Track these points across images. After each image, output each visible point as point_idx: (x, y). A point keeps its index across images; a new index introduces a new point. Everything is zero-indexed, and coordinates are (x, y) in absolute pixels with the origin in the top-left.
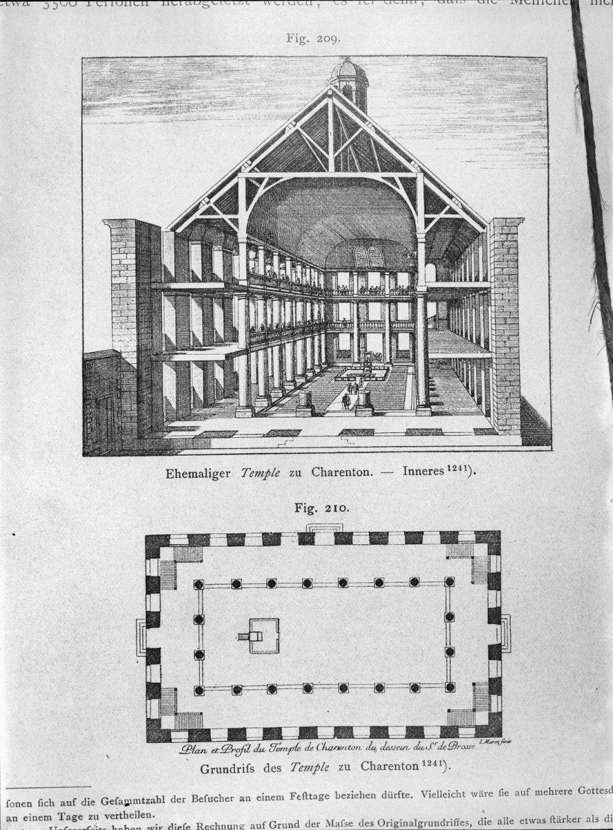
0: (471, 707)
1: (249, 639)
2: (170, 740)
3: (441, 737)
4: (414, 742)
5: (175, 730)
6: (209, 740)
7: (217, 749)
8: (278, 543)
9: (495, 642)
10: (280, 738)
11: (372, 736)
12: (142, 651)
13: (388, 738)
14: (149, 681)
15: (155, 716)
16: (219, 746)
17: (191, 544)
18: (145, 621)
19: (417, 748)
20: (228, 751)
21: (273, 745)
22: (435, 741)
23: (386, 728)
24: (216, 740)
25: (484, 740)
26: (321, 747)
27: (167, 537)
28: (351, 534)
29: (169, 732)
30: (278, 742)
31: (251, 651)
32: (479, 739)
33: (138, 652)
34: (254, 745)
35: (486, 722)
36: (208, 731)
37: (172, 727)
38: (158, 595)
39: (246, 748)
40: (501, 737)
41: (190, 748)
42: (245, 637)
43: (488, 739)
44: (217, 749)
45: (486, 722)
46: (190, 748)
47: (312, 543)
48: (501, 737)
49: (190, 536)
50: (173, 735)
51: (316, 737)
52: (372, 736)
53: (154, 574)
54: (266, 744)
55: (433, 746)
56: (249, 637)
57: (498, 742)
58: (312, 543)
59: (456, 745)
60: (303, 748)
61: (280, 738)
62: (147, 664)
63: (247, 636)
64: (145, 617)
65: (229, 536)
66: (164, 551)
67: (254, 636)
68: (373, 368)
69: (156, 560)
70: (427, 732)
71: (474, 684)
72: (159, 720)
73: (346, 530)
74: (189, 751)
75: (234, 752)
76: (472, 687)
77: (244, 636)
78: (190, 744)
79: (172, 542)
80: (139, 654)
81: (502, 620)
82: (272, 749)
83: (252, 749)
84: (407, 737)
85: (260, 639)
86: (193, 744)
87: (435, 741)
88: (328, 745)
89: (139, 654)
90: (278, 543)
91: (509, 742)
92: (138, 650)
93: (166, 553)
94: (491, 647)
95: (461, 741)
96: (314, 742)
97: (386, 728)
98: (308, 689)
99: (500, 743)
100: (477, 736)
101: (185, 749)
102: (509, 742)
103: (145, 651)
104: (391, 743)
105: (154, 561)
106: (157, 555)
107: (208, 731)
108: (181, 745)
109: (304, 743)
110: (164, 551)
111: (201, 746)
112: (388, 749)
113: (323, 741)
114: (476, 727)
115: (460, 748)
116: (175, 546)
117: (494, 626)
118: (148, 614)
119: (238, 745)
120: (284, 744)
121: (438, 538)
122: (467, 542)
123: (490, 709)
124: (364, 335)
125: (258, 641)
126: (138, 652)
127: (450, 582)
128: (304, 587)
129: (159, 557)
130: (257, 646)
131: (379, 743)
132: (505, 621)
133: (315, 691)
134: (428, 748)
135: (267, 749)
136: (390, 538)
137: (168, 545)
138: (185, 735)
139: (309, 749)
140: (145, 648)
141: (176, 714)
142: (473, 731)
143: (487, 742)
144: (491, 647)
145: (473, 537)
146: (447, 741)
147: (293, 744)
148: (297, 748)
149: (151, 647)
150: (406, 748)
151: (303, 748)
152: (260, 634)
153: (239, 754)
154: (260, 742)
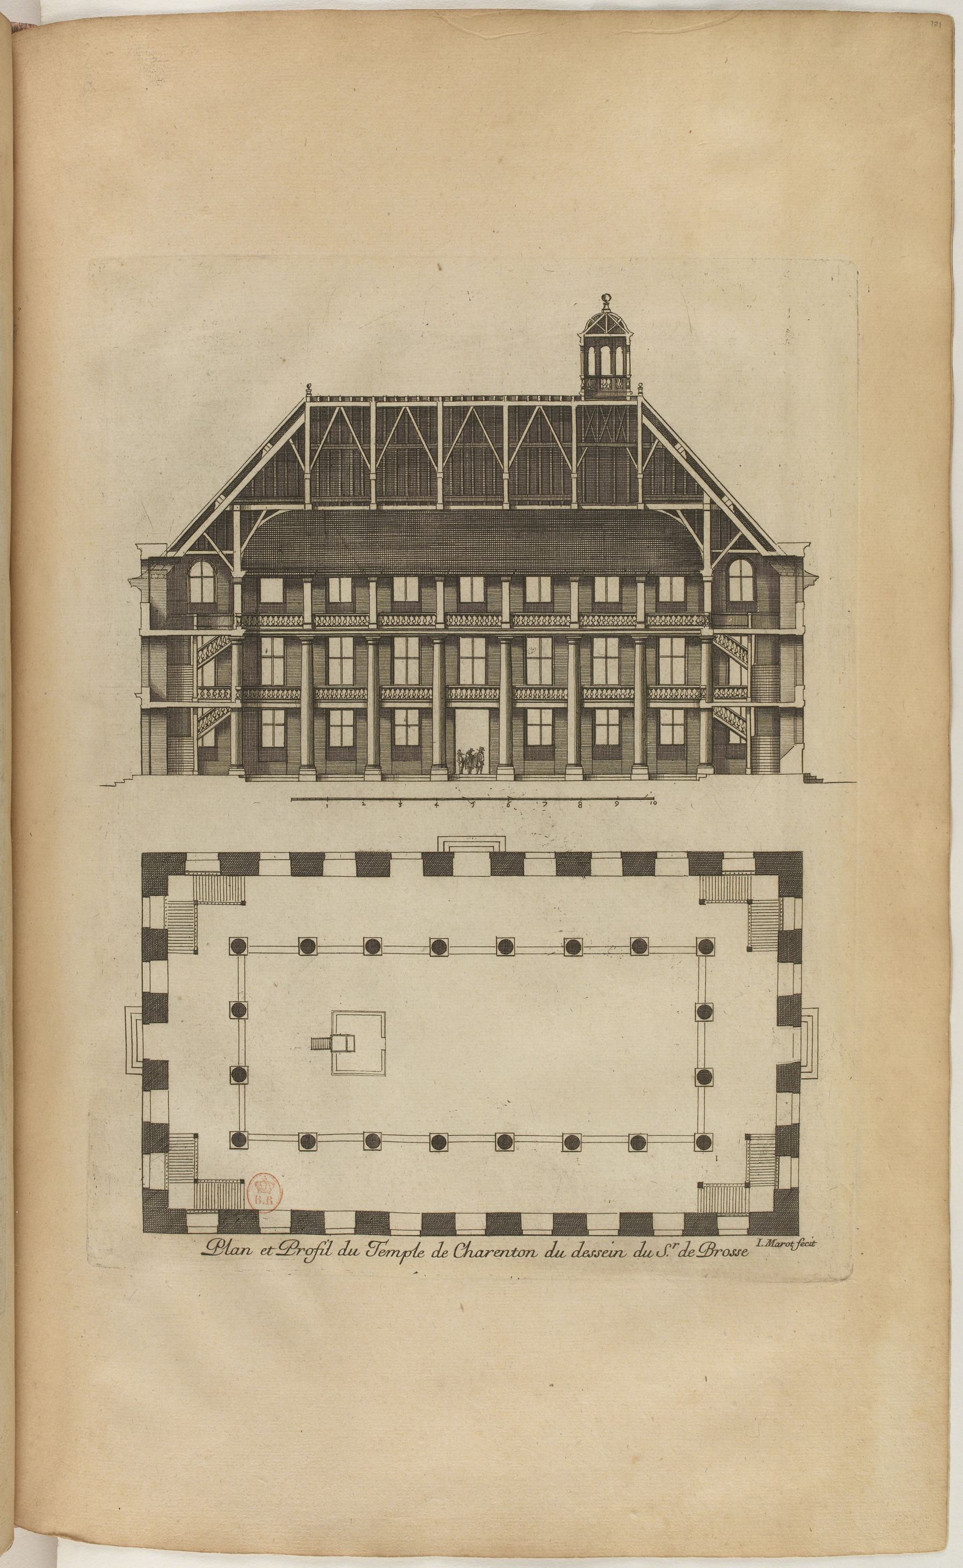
0: (742, 1180)
1: (331, 1048)
2: (184, 1230)
3: (685, 1233)
4: (636, 1242)
6: (257, 1230)
7: (271, 1248)
9: (789, 1059)
10: (386, 1231)
13: (587, 1234)
15: (157, 1183)
16: (275, 1241)
18: (140, 1010)
19: (642, 1253)
20: (291, 1252)
21: (372, 1245)
22: (671, 1241)
23: (583, 1217)
24: (268, 1231)
25: (765, 1239)
26: (461, 1252)
27: (181, 858)
28: (522, 855)
29: (183, 1213)
31: (336, 1072)
32: (754, 1239)
33: (129, 1065)
35: (769, 1207)
37: (189, 1206)
39: (325, 1247)
40: (797, 1234)
41: (221, 1245)
42: (322, 1044)
43: (772, 1238)
44: (271, 1248)
45: (769, 1207)
46: (221, 1245)
48: (797, 1234)
49: (222, 856)
50: (191, 1220)
51: (453, 1232)
52: (555, 1232)
53: (157, 924)
54: (361, 1241)
56: (331, 1044)
57: (791, 1244)
59: (713, 1250)
60: (428, 1254)
61: (386, 1231)
63: (327, 1041)
64: (139, 1003)
66: (174, 882)
67: (338, 1044)
68: (199, 903)
71: (748, 1137)
73: (511, 848)
74: (219, 1250)
80: (441, 840)
81: (803, 1019)
82: (372, 1251)
83: (335, 1249)
84: (622, 1232)
85: (351, 1048)
86: (227, 1237)
87: (671, 1241)
88: (474, 1248)
89: (441, 840)
91: (812, 1244)
92: (448, 839)
93: (179, 887)
95: (722, 1243)
97: (583, 1217)
98: (439, 1143)
99: (795, 1246)
100: (750, 1232)
101: (212, 1246)
102: (812, 1244)
103: (141, 1065)
104: (591, 1243)
105: (157, 901)
106: (162, 890)
108: (205, 1239)
109: (431, 1243)
110: (174, 882)
111: (240, 1240)
113: (466, 1240)
114: (751, 1215)
115: (720, 1253)
116: (195, 874)
117: (788, 1031)
118: (146, 996)
119: (309, 1241)
120: (394, 1243)
122: (740, 873)
123: (777, 1181)
124: (327, 713)
125: (347, 1051)
126: (129, 1065)
127: (706, 947)
128: (433, 954)
129: (166, 894)
130: (344, 1061)
131: (568, 1243)
133: (710, 1064)
136: (594, 864)
137: (183, 873)
138: (213, 1220)
139: (439, 1254)
140: (140, 1059)
141: (196, 1181)
142: (744, 1222)
143: (771, 1243)
145: (751, 865)
146: (697, 1241)
147: (408, 1244)
148: (416, 1252)
149: (153, 1058)
150: (620, 1253)
151: (428, 1254)
152: (350, 1040)
153: (310, 1258)
154: (348, 1238)
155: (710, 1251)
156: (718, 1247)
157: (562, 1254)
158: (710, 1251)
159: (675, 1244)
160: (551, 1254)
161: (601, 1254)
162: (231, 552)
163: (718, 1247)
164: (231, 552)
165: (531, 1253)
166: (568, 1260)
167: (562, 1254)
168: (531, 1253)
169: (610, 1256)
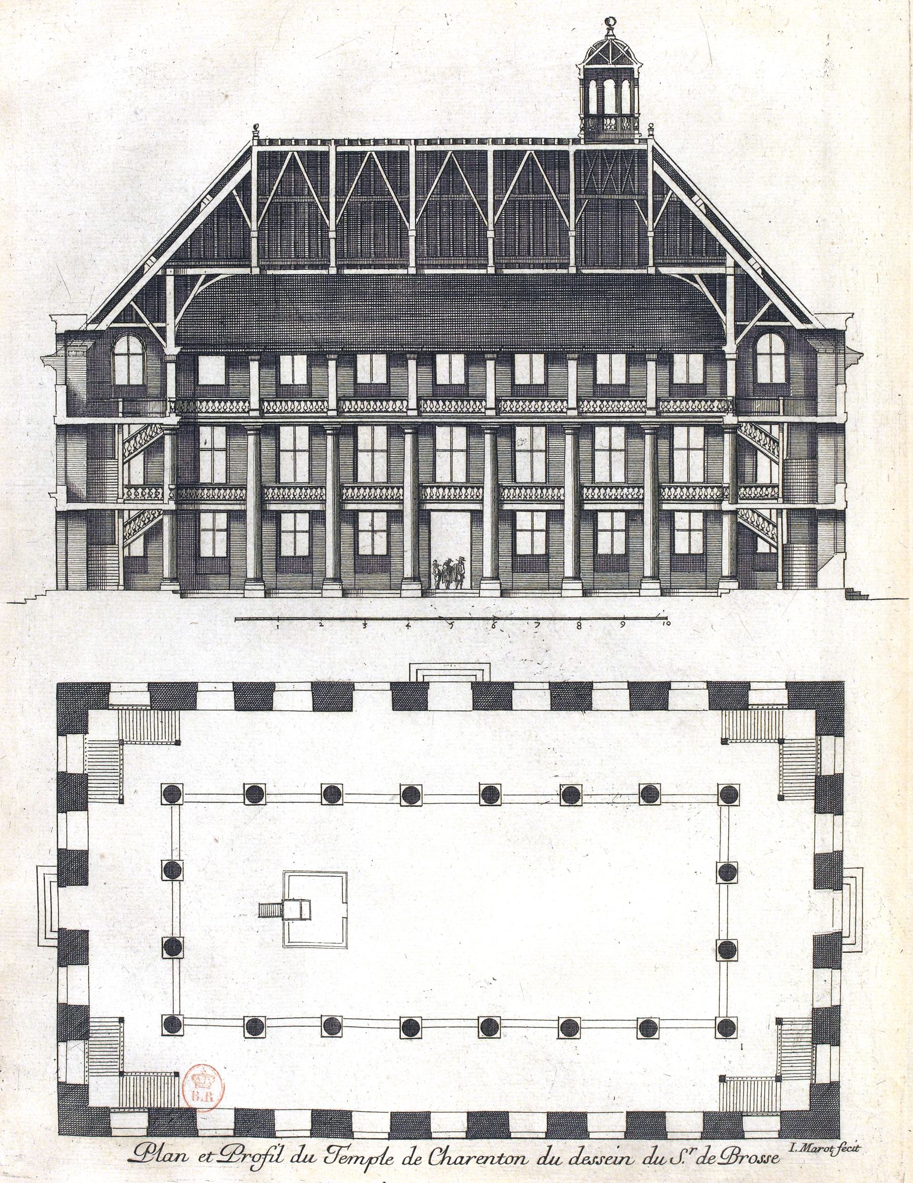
0: (772, 1072)
1: (282, 916)
2: (107, 1132)
3: (705, 1136)
4: (645, 1146)
5: (121, 1110)
6: (193, 1132)
7: (210, 1154)
8: (347, 706)
10: (348, 1133)
11: (550, 1134)
12: (49, 935)
13: (588, 1138)
14: (62, 1000)
15: (75, 1077)
16: (215, 1145)
17: (156, 705)
18: (55, 870)
19: (653, 1160)
20: (234, 1158)
21: (332, 1150)
22: (688, 1145)
23: (583, 1116)
24: (208, 1133)
25: (800, 1143)
26: (437, 1158)
27: (104, 689)
28: (510, 686)
29: (105, 1112)
30: (344, 1142)
32: (787, 1143)
33: (42, 935)
34: (292, 1148)
36: (713, 705)
38: (84, 813)
39: (275, 1152)
40: (838, 1137)
43: (808, 1141)
44: (210, 1154)
46: (151, 1149)
47: (422, 705)
48: (838, 1137)
50: (116, 1120)
52: (550, 1134)
53: (75, 767)
54: (318, 1146)
55: (684, 1155)
56: (282, 910)
57: (831, 1149)
58: (422, 705)
59: (738, 1156)
60: (398, 1160)
61: (348, 1133)
62: (840, 854)
63: (278, 907)
65: (238, 688)
66: (96, 717)
67: (291, 910)
69: (80, 737)
70: (672, 1122)
72: (85, 1088)
74: (149, 1156)
75: (248, 1159)
76: (774, 1027)
77: (271, 908)
78: (150, 1139)
79: (114, 699)
81: (845, 881)
82: (331, 1158)
83: (287, 1155)
84: (630, 1134)
85: (306, 915)
86: (158, 1141)
87: (688, 1145)
88: (453, 1154)
90: (347, 706)
91: (856, 1149)
94: (83, 880)
95: (747, 1147)
96: (424, 1147)
97: (583, 1116)
99: (835, 1151)
100: (782, 1135)
101: (141, 1151)
102: (856, 1149)
103: (56, 935)
105: (75, 740)
107: (713, 705)
108: (132, 1143)
109: (401, 1148)
112: (588, 1161)
114: (783, 1115)
116: (120, 708)
117: (826, 895)
118: (63, 855)
119: (256, 1145)
120: (357, 1148)
121: (702, 698)
123: (813, 1074)
125: (301, 919)
126: (42, 935)
129: (86, 733)
130: (298, 931)
131: (565, 1148)
132: (852, 881)
134: (676, 1160)
135: (319, 1157)
137: (107, 707)
138: (142, 1120)
139: (411, 1161)
141: (121, 1074)
142: (775, 1123)
143: (806, 1148)
144: (83, 880)
145: (782, 697)
146: (718, 1146)
147: (374, 1149)
148: (384, 1159)
151: (398, 1160)
152: (305, 905)
153: (257, 1166)
154: (302, 1141)
155: (734, 1157)
156: (743, 1153)
157: (557, 1161)
158: (734, 1157)
159: (693, 1149)
160: (544, 1160)
161: (604, 1160)
162: (163, 325)
163: (743, 1153)
164: (163, 325)
165: (521, 1160)
166: (565, 1168)
167: (557, 1161)
168: (521, 1160)
169: (614, 1163)
